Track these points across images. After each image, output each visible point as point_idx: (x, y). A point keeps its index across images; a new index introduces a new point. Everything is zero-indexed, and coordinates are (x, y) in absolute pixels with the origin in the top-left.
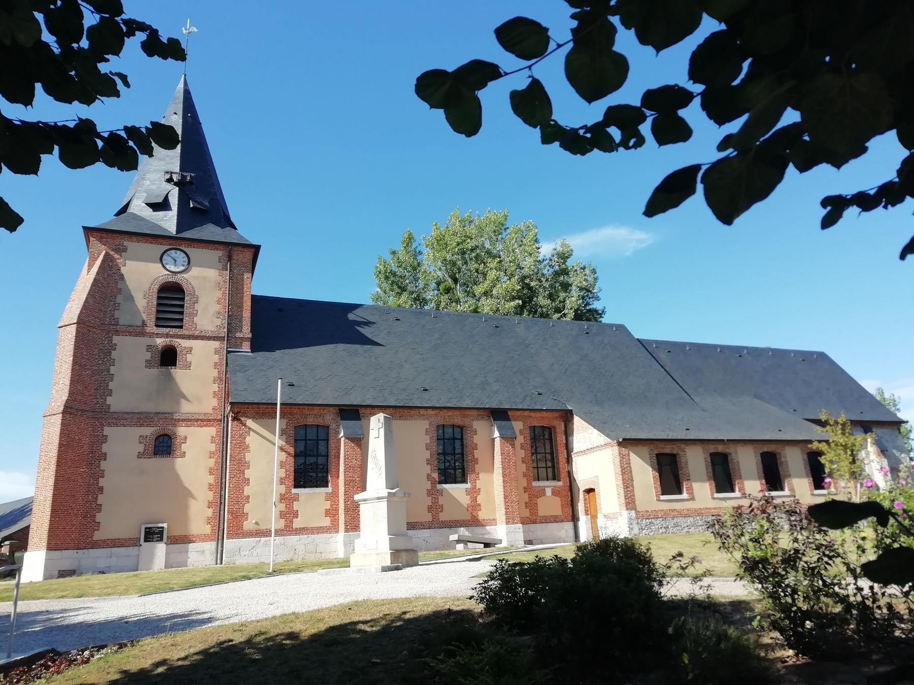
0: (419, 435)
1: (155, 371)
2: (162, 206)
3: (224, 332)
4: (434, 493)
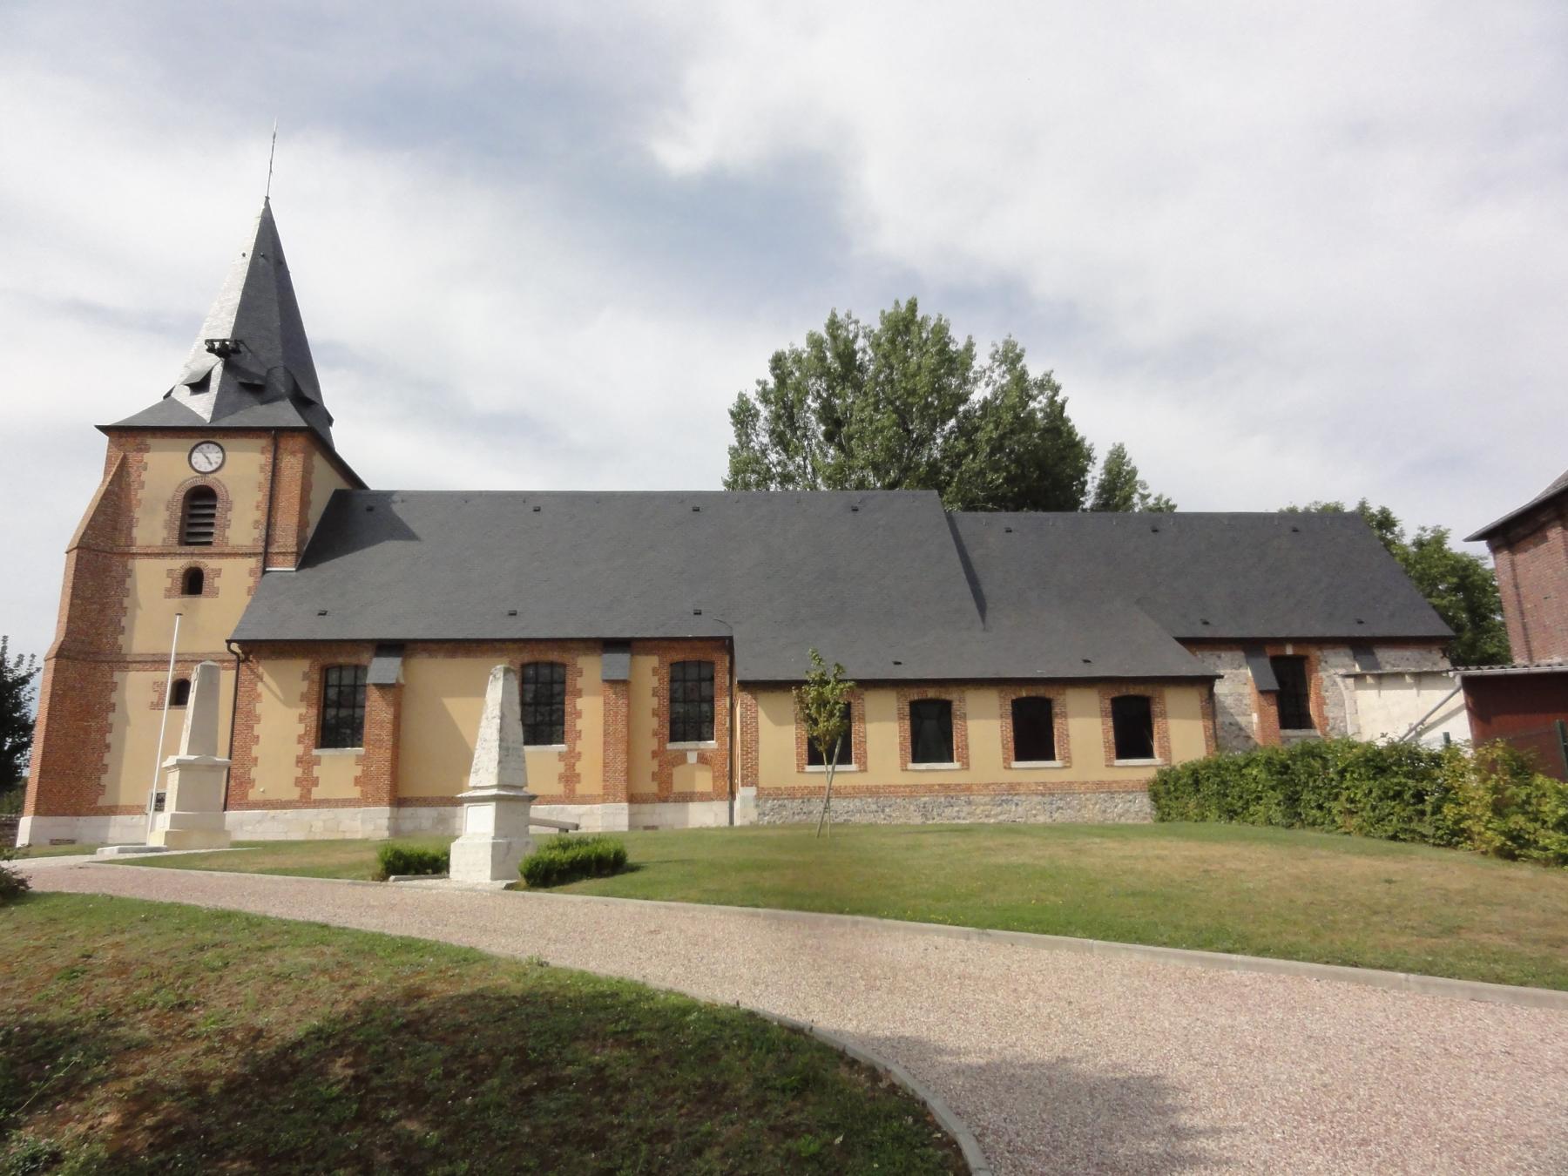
0: (649, 673)
1: (179, 602)
2: (199, 386)
3: (261, 550)
4: (305, 762)
